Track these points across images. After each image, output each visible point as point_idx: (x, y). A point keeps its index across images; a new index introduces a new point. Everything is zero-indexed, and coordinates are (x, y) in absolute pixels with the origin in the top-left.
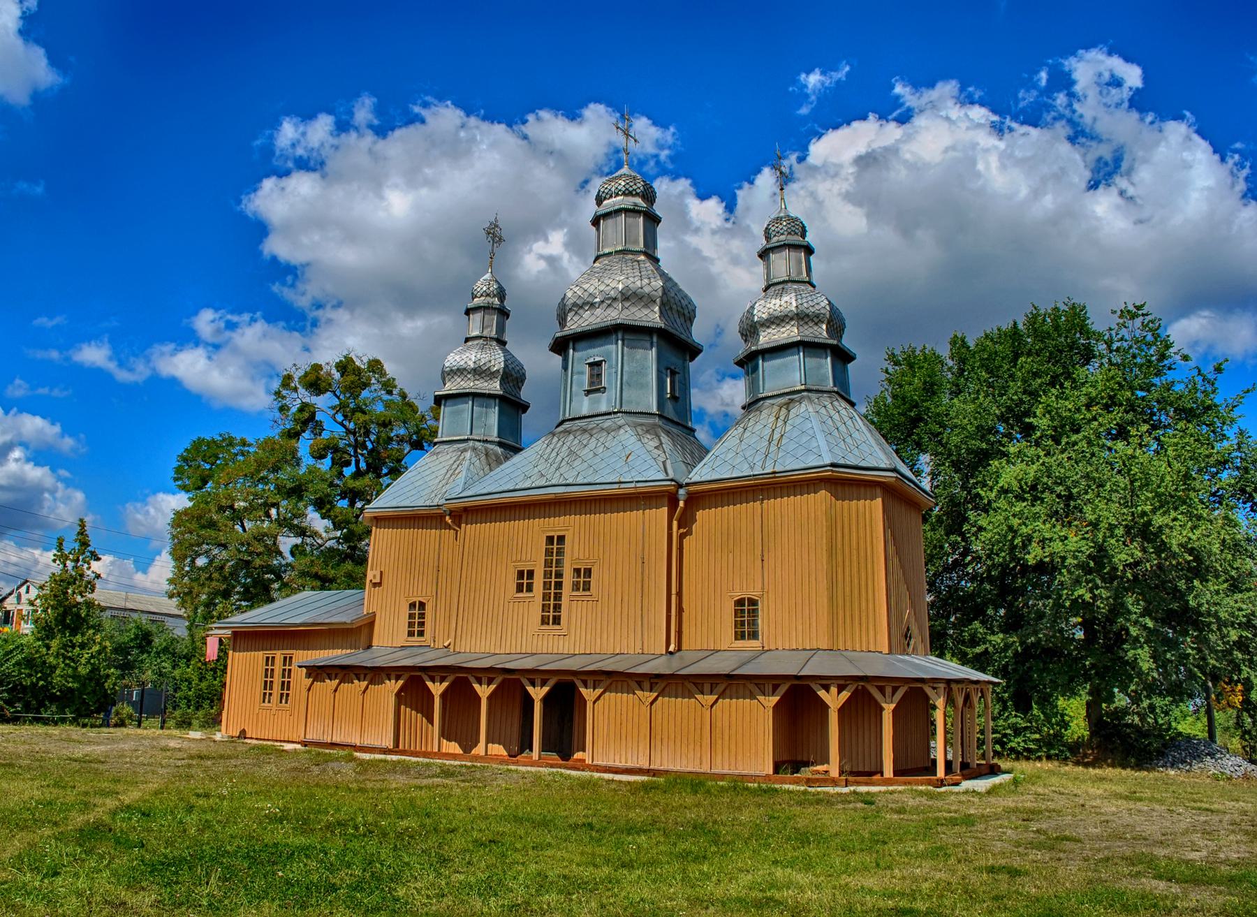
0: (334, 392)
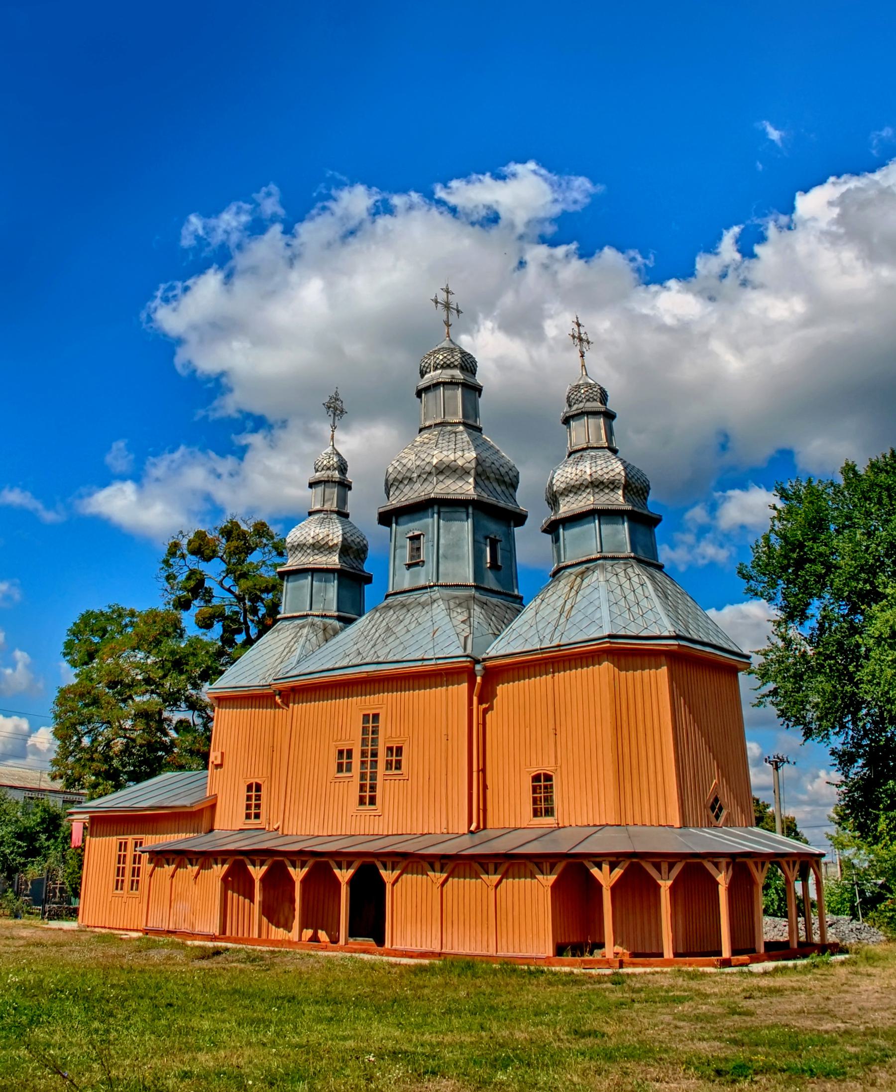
0: (221, 558)
